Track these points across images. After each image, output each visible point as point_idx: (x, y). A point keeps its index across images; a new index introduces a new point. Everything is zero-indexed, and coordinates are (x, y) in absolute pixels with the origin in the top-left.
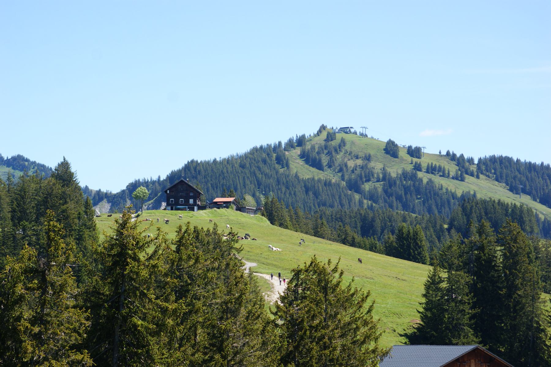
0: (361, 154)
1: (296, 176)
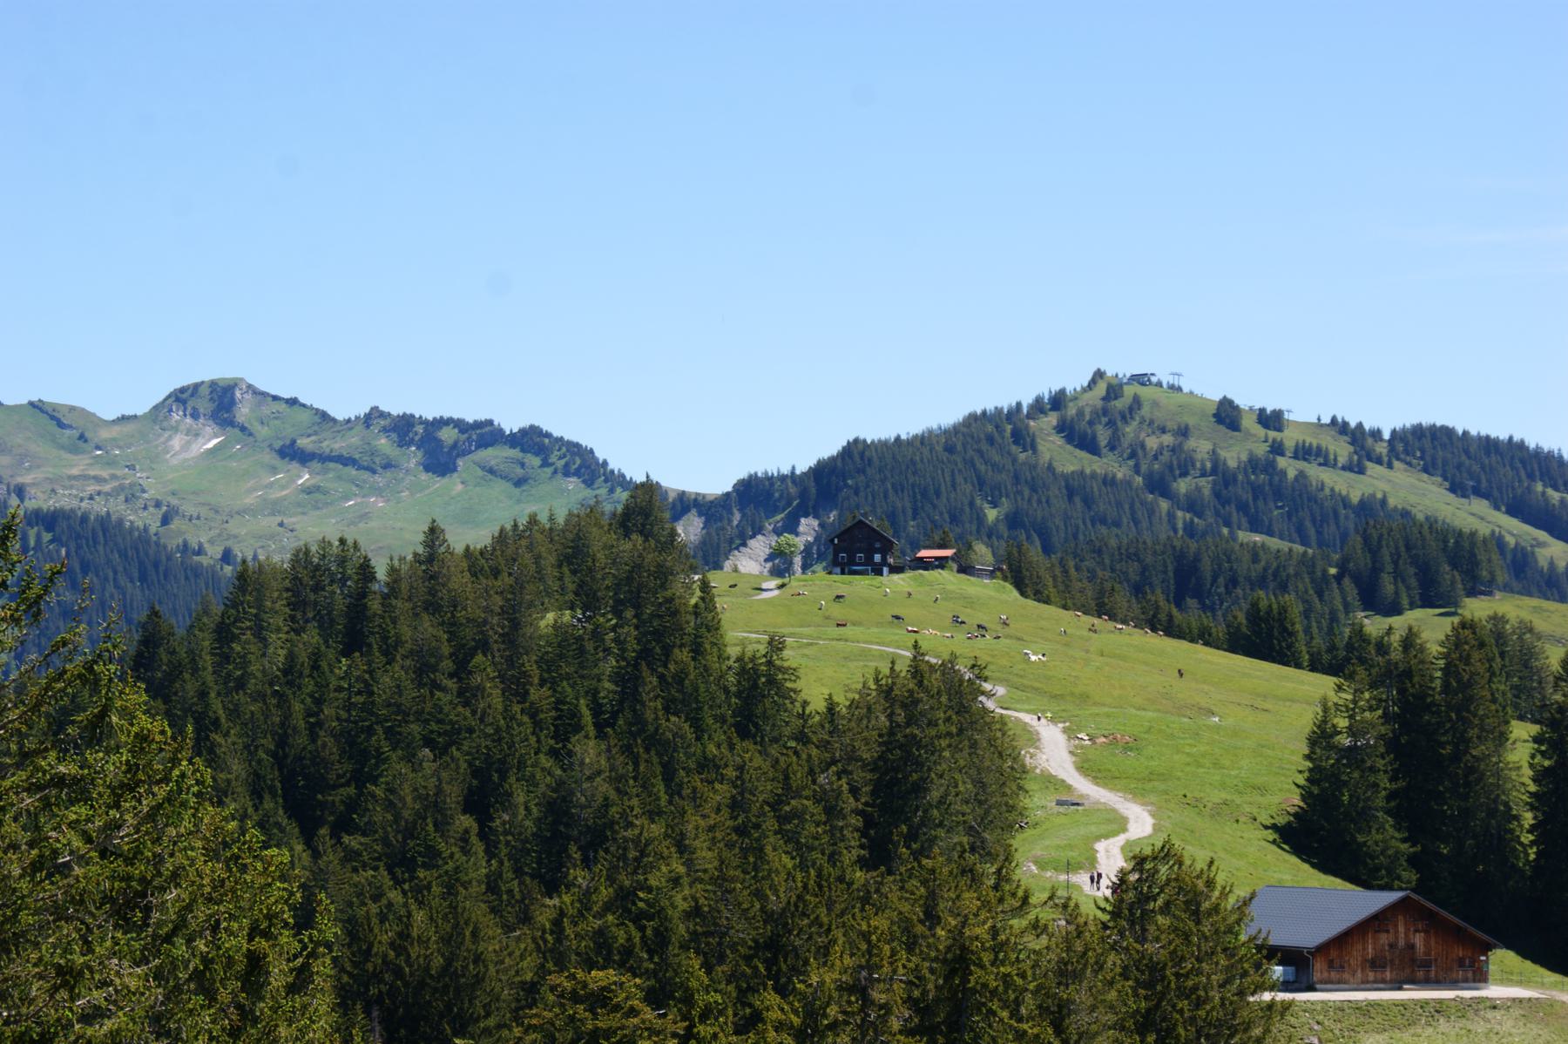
0: (1170, 425)
1: (1050, 468)
